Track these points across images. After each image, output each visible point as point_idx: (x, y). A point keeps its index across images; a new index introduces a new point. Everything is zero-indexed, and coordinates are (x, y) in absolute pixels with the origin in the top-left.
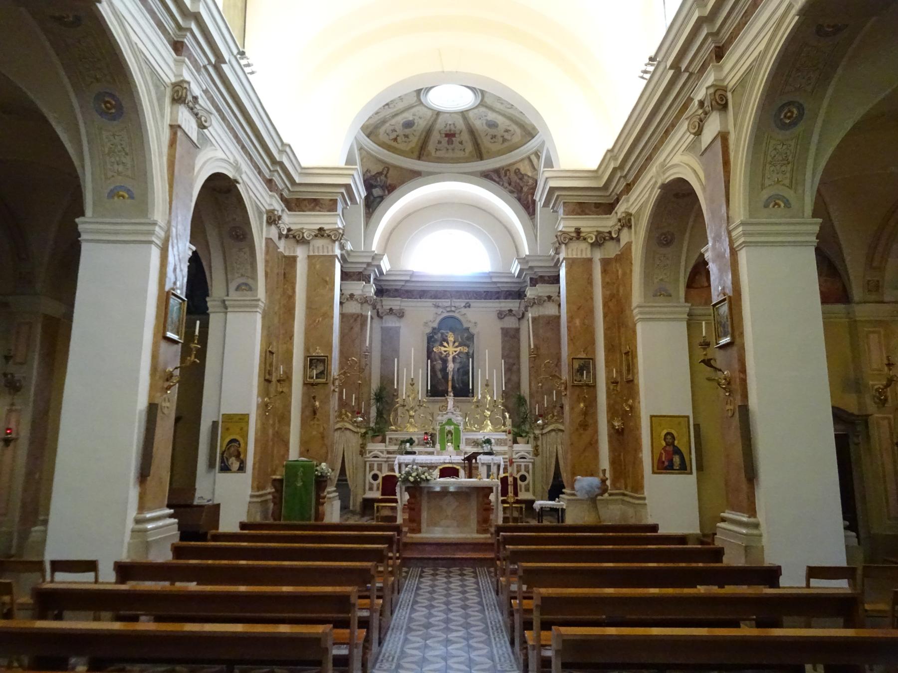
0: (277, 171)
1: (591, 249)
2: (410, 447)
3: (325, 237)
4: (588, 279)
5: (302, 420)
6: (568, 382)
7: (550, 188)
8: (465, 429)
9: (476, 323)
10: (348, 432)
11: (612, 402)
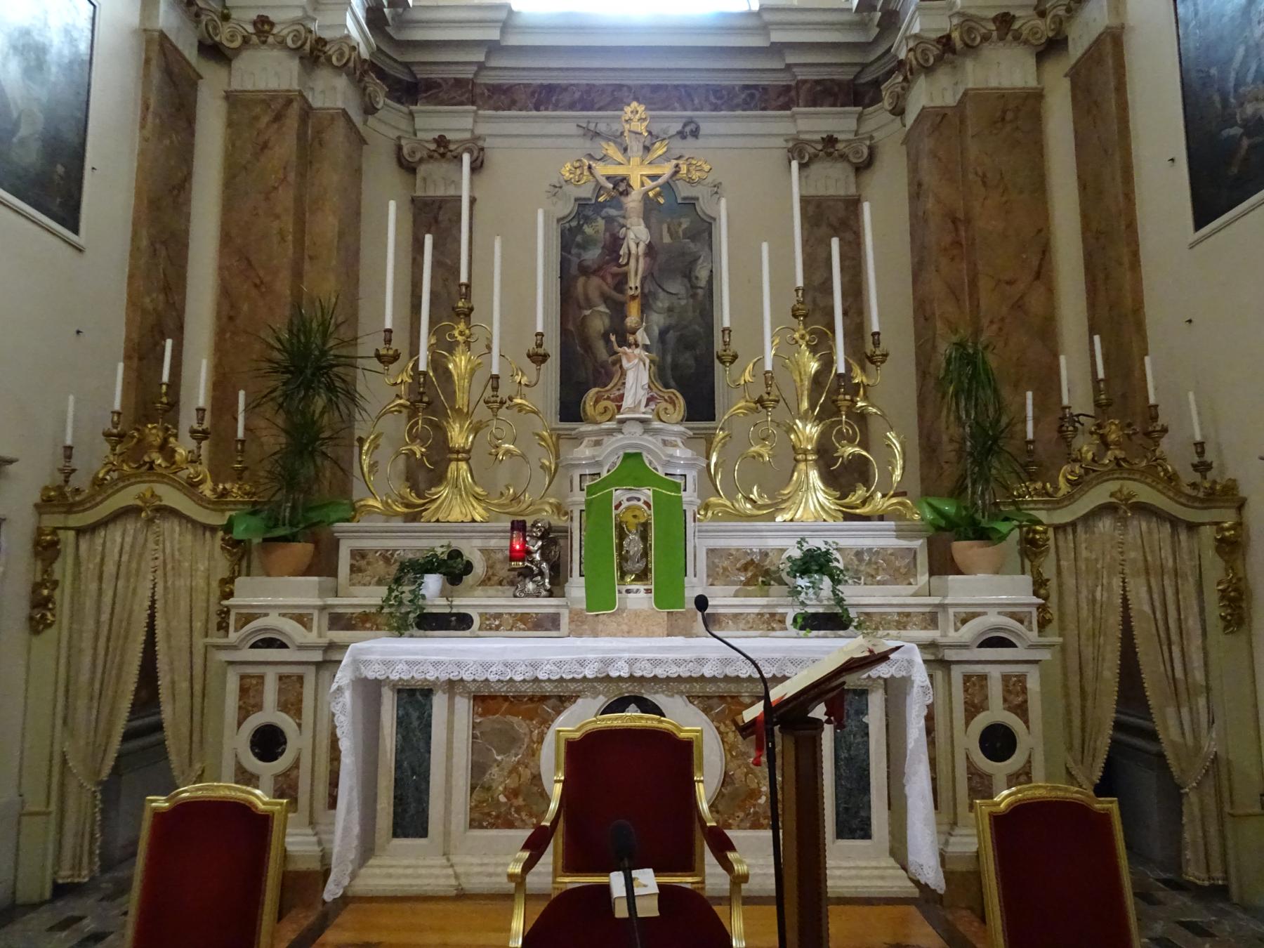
2: (443, 594)
10: (169, 527)
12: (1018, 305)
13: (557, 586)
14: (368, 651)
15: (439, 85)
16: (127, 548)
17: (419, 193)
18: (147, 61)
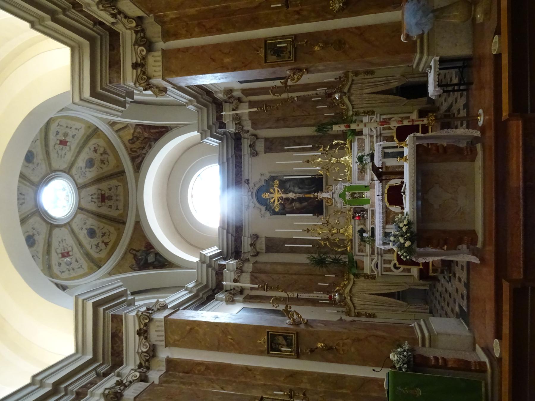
0: (66, 388)
1: (155, 51)
2: (367, 233)
3: (147, 328)
4: (183, 51)
5: (337, 362)
6: (293, 67)
7: (92, 95)
8: (349, 181)
9: (261, 175)
10: (354, 290)
11: (313, 15)
12: (299, 106)
13: (366, 210)
14: (377, 243)
15: (236, 246)
16: (358, 299)
17: (264, 251)
18: (249, 302)
